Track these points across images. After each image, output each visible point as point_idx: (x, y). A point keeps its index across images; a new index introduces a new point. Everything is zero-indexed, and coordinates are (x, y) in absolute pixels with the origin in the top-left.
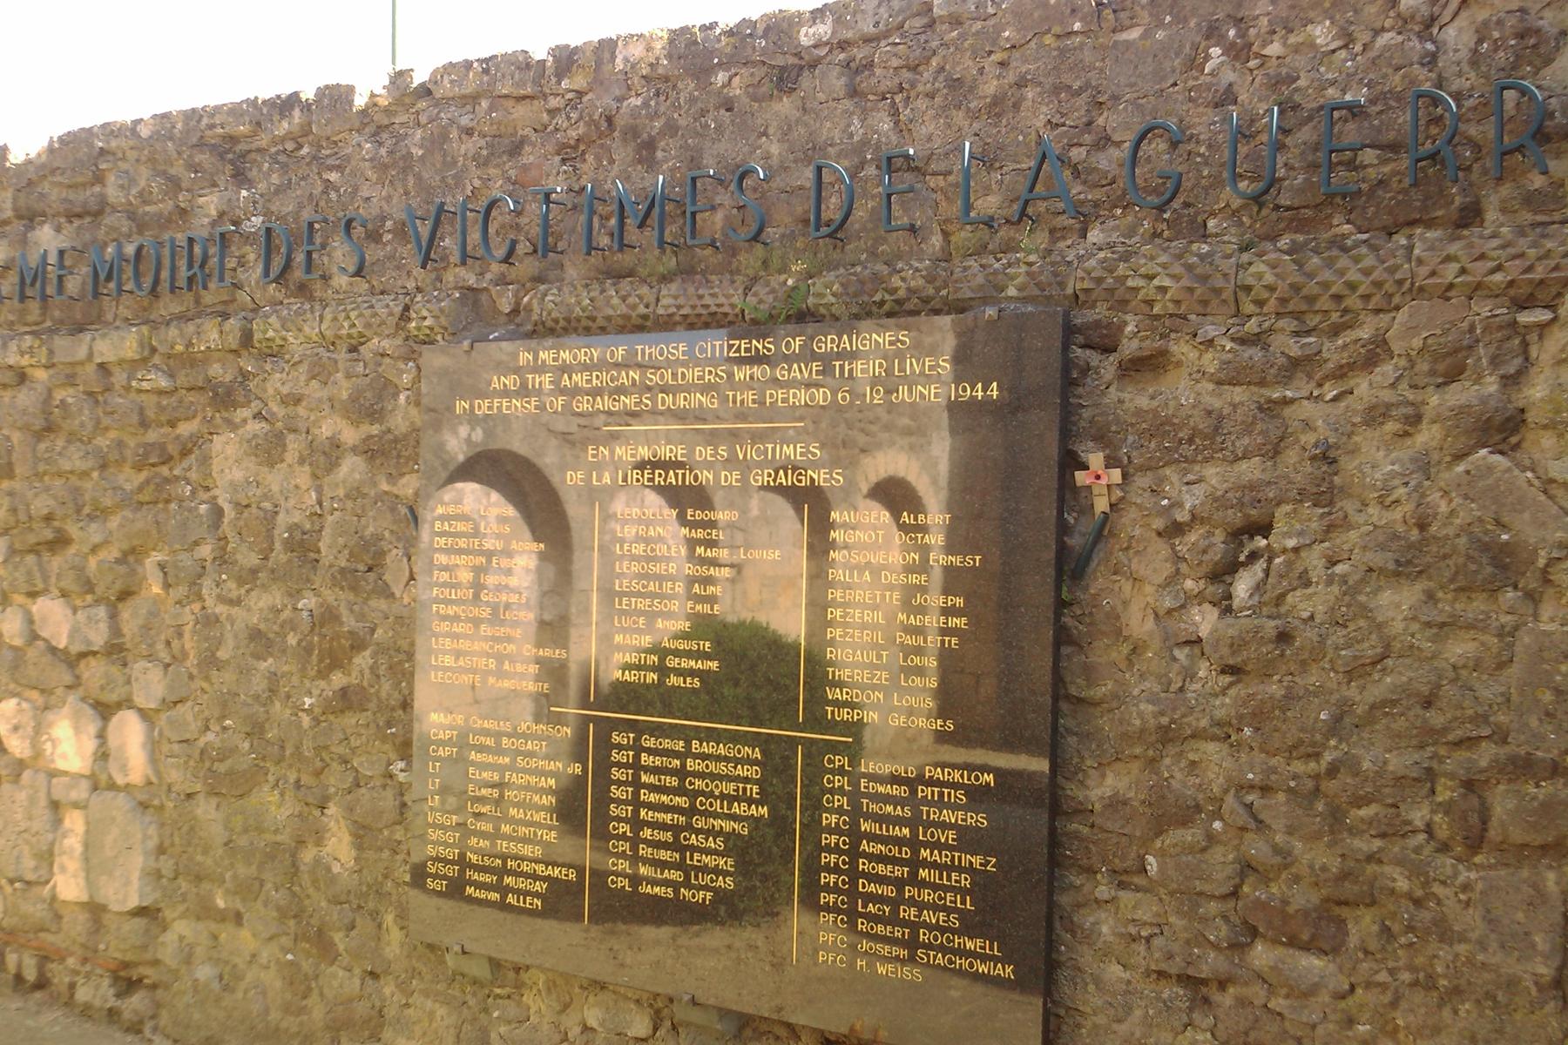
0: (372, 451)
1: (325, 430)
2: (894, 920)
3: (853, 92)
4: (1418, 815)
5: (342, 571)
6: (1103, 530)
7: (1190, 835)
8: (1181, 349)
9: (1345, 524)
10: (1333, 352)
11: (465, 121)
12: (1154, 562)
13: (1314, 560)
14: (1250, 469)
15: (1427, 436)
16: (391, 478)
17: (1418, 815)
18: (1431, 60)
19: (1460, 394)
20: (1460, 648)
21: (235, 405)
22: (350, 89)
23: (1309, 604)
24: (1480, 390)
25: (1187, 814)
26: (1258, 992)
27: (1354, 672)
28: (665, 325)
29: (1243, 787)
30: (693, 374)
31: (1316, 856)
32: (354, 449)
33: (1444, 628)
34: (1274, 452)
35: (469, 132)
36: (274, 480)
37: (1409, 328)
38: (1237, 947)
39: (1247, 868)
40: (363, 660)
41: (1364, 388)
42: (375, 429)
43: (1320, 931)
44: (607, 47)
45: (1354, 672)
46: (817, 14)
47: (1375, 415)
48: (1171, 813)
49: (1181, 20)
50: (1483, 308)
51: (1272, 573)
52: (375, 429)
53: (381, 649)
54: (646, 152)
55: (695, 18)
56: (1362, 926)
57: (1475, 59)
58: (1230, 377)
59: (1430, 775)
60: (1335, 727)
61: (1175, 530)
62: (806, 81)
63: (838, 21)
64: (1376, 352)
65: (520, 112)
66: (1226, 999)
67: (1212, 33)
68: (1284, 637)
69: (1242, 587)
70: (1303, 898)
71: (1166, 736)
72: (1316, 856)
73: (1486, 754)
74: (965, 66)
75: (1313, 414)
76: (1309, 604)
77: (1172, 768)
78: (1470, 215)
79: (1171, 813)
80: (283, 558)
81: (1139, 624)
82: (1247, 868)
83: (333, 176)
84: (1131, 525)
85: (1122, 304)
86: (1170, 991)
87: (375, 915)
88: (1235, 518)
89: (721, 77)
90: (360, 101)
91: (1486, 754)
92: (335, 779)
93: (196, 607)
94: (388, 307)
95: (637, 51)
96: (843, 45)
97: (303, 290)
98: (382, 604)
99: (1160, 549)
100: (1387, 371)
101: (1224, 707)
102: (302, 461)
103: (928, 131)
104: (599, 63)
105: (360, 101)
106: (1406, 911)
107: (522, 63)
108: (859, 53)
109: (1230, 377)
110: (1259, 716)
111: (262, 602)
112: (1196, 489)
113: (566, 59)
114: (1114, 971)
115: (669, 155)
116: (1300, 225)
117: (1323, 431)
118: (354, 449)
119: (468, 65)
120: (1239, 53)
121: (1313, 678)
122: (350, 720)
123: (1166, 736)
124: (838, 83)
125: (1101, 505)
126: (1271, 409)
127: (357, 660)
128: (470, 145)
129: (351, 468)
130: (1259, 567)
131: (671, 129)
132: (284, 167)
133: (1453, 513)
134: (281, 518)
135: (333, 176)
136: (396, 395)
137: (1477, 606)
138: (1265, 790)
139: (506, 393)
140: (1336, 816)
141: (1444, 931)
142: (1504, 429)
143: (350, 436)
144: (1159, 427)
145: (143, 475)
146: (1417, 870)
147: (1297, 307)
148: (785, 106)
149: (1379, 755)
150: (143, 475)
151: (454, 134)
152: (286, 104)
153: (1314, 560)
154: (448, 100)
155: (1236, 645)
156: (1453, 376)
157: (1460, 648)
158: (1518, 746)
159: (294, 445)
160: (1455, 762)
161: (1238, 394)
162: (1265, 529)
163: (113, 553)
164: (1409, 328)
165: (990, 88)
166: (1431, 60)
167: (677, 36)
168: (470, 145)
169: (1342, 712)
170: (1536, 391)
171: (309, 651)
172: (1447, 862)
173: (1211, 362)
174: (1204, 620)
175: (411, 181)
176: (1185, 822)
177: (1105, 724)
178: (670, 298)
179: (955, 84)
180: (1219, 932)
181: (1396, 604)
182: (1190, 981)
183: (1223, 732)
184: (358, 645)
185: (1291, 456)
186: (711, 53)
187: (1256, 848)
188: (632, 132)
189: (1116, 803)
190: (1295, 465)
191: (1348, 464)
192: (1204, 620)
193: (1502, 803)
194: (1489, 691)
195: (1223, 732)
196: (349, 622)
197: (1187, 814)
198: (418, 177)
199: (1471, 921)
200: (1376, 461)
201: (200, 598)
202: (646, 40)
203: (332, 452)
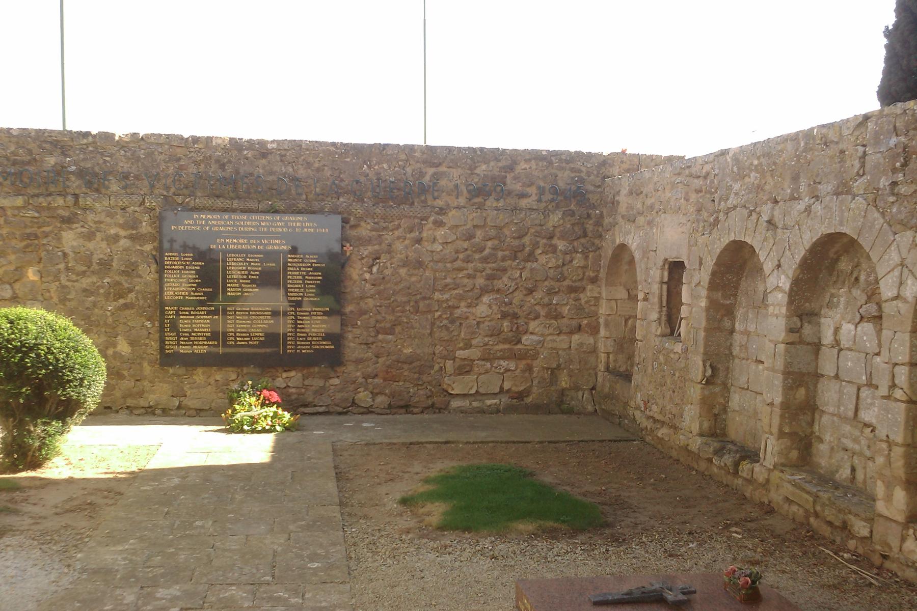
0: (132, 238)
1: (112, 232)
2: (307, 341)
3: (282, 161)
4: (408, 308)
5: (123, 271)
6: (348, 259)
7: (367, 316)
8: (363, 224)
9: (393, 257)
10: (391, 226)
11: (160, 150)
12: (358, 265)
13: (388, 264)
14: (377, 247)
15: (407, 242)
16: (141, 246)
17: (408, 308)
18: (405, 174)
19: (413, 235)
20: (414, 279)
21: (73, 223)
22: (114, 135)
23: (388, 272)
24: (415, 234)
25: (365, 312)
26: (380, 344)
27: (396, 284)
28: (234, 211)
29: (377, 306)
30: (249, 223)
31: (390, 317)
32: (125, 237)
33: (411, 275)
34: (380, 244)
35: (161, 153)
36: (91, 245)
37: (405, 223)
38: (376, 336)
39: (377, 321)
40: (132, 296)
41: (397, 233)
42: (134, 232)
43: (390, 331)
44: (209, 139)
45: (396, 284)
46: (273, 142)
47: (398, 238)
48: (362, 313)
49: (358, 158)
50: (416, 220)
51: (768, 250)
52: (134, 232)
53: (138, 292)
54: (222, 166)
55: (237, 135)
56: (398, 329)
57: (412, 175)
58: (372, 230)
59: (409, 301)
60: (393, 294)
61: (363, 258)
62: (270, 156)
63: (278, 144)
64: (399, 226)
65: (179, 150)
66: (374, 346)
67: (365, 163)
68: (384, 278)
69: (375, 269)
70: (388, 325)
71: (361, 298)
72: (390, 317)
73: (418, 297)
74: (311, 159)
75: (388, 237)
76: (388, 272)
77: (362, 304)
78: (413, 203)
79: (362, 313)
80: (97, 267)
81: (355, 276)
82: (377, 321)
83: (107, 159)
84: (354, 258)
85: (350, 214)
86: (363, 346)
87: (140, 364)
88: (374, 257)
89: (245, 152)
90: (117, 138)
91: (418, 297)
92: (120, 329)
93: (57, 283)
94: (137, 199)
95: (220, 142)
96: (279, 150)
97: (97, 191)
98: (139, 280)
99: (359, 262)
100: (401, 230)
101: (372, 292)
102: (102, 240)
103: (302, 172)
104: (207, 142)
105: (117, 138)
106: (406, 325)
107: (181, 138)
108: (283, 153)
109: (372, 230)
110: (379, 293)
111: (85, 282)
112: (366, 251)
113: (196, 140)
114: (352, 345)
115: (229, 169)
116: (383, 202)
117: (389, 240)
118: (125, 237)
119: (161, 135)
120: (369, 167)
121: (389, 285)
122: (127, 312)
123: (361, 298)
124: (278, 158)
125: (348, 254)
126: (380, 236)
127: (130, 295)
128: (162, 157)
129: (124, 243)
130: (377, 266)
131: (230, 162)
132: (85, 153)
133: (412, 255)
134: (95, 256)
135: (107, 159)
136: (141, 223)
137: (416, 272)
138: (380, 306)
139: (189, 225)
140: (393, 311)
141: (413, 328)
142: (419, 241)
143: (122, 233)
144: (359, 239)
145: (25, 243)
146: (408, 318)
147: (384, 218)
148: (264, 161)
149: (401, 298)
150: (25, 243)
151: (156, 153)
152: (87, 134)
153: (388, 264)
154: (152, 143)
155: (375, 280)
156: (411, 232)
157: (414, 279)
158: (423, 295)
159: (99, 236)
160: (413, 298)
161: (374, 233)
162: (378, 258)
163: (12, 268)
164: (405, 223)
165: (316, 165)
166: (405, 174)
167: (231, 140)
168: (162, 157)
169: (394, 291)
170: (424, 235)
171: (109, 294)
172: (412, 316)
173: (369, 227)
174: (367, 276)
175: (140, 164)
176: (365, 314)
177: (349, 297)
178: (236, 204)
179: (308, 163)
180: (373, 334)
181: (403, 271)
182: (366, 344)
183: (372, 297)
184: (130, 291)
185: (383, 245)
186: (243, 146)
187: (379, 317)
188: (217, 161)
189: (352, 312)
190: (384, 246)
191: (394, 246)
192: (367, 276)
193: (421, 304)
194: (419, 286)
195: (372, 297)
196: (126, 285)
197: (365, 312)
198: (143, 164)
199: (417, 325)
200: (399, 246)
201: (59, 280)
202: (224, 140)
203: (116, 238)
